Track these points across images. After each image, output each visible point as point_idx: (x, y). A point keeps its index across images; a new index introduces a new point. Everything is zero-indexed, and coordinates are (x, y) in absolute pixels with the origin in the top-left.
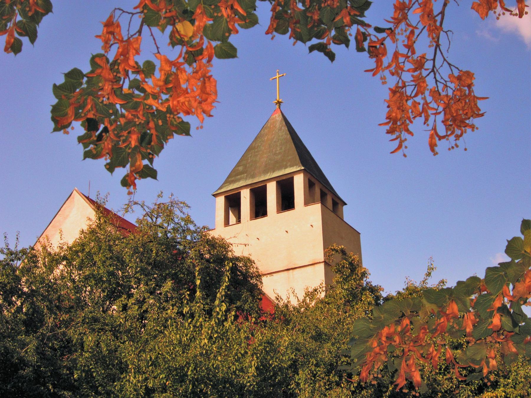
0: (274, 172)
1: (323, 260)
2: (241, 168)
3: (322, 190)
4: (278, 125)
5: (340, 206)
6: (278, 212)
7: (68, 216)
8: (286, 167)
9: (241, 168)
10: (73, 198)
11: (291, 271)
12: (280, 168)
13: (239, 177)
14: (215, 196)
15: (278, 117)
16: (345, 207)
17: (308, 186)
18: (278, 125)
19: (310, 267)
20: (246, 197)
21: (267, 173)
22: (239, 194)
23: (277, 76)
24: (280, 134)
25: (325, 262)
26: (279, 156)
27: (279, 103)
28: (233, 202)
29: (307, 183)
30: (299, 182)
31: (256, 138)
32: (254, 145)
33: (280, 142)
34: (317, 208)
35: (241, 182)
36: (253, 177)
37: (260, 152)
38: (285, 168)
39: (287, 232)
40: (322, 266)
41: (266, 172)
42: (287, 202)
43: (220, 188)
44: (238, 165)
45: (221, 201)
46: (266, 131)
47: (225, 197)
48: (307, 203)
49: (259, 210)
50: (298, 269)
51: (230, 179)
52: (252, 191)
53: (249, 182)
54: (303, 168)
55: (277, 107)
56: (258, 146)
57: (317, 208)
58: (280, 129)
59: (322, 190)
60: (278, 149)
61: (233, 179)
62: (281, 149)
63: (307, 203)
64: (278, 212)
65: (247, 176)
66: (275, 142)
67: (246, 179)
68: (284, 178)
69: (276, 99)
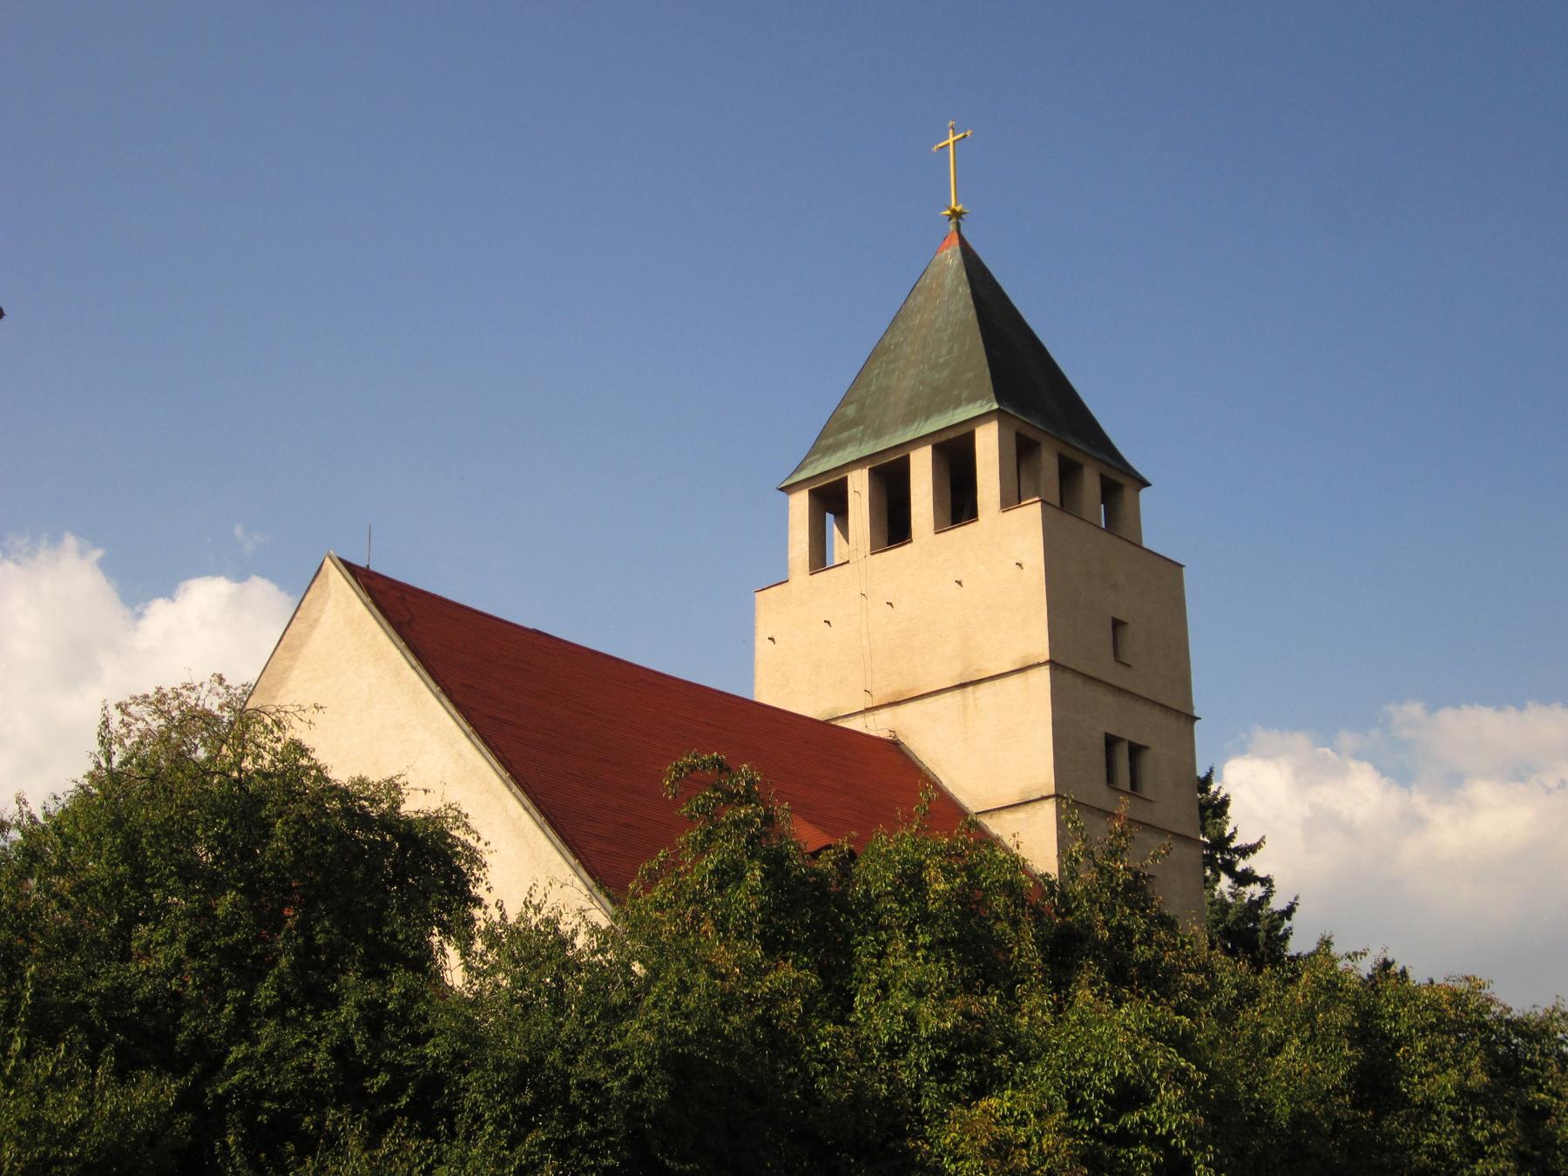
0: (927, 418)
1: (1047, 657)
2: (851, 411)
3: (1069, 457)
4: (949, 281)
5: (1127, 493)
6: (939, 528)
7: (317, 620)
8: (957, 404)
9: (851, 411)
10: (326, 576)
11: (970, 689)
12: (942, 408)
13: (845, 434)
14: (788, 489)
15: (951, 257)
16: (1144, 492)
17: (1013, 452)
18: (948, 280)
19: (1015, 677)
20: (859, 485)
21: (913, 422)
22: (843, 483)
23: (951, 140)
24: (953, 308)
25: (1056, 665)
26: (945, 373)
27: (957, 215)
28: (829, 500)
29: (1013, 446)
30: (987, 442)
31: (894, 322)
32: (886, 342)
33: (950, 330)
34: (1031, 514)
35: (849, 450)
36: (878, 434)
37: (901, 363)
38: (955, 408)
39: (959, 583)
40: (1044, 674)
41: (908, 419)
42: (959, 505)
43: (798, 470)
44: (844, 403)
45: (800, 503)
46: (920, 299)
47: (811, 492)
48: (1011, 499)
49: (893, 527)
50: (986, 684)
51: (824, 442)
52: (874, 473)
53: (867, 449)
54: (996, 406)
55: (952, 227)
56: (896, 345)
57: (1031, 514)
58: (954, 293)
59: (1069, 457)
60: (944, 351)
61: (831, 440)
62: (950, 351)
63: (1011, 499)
64: (939, 528)
65: (864, 432)
66: (937, 331)
67: (861, 441)
68: (952, 435)
69: (948, 207)
